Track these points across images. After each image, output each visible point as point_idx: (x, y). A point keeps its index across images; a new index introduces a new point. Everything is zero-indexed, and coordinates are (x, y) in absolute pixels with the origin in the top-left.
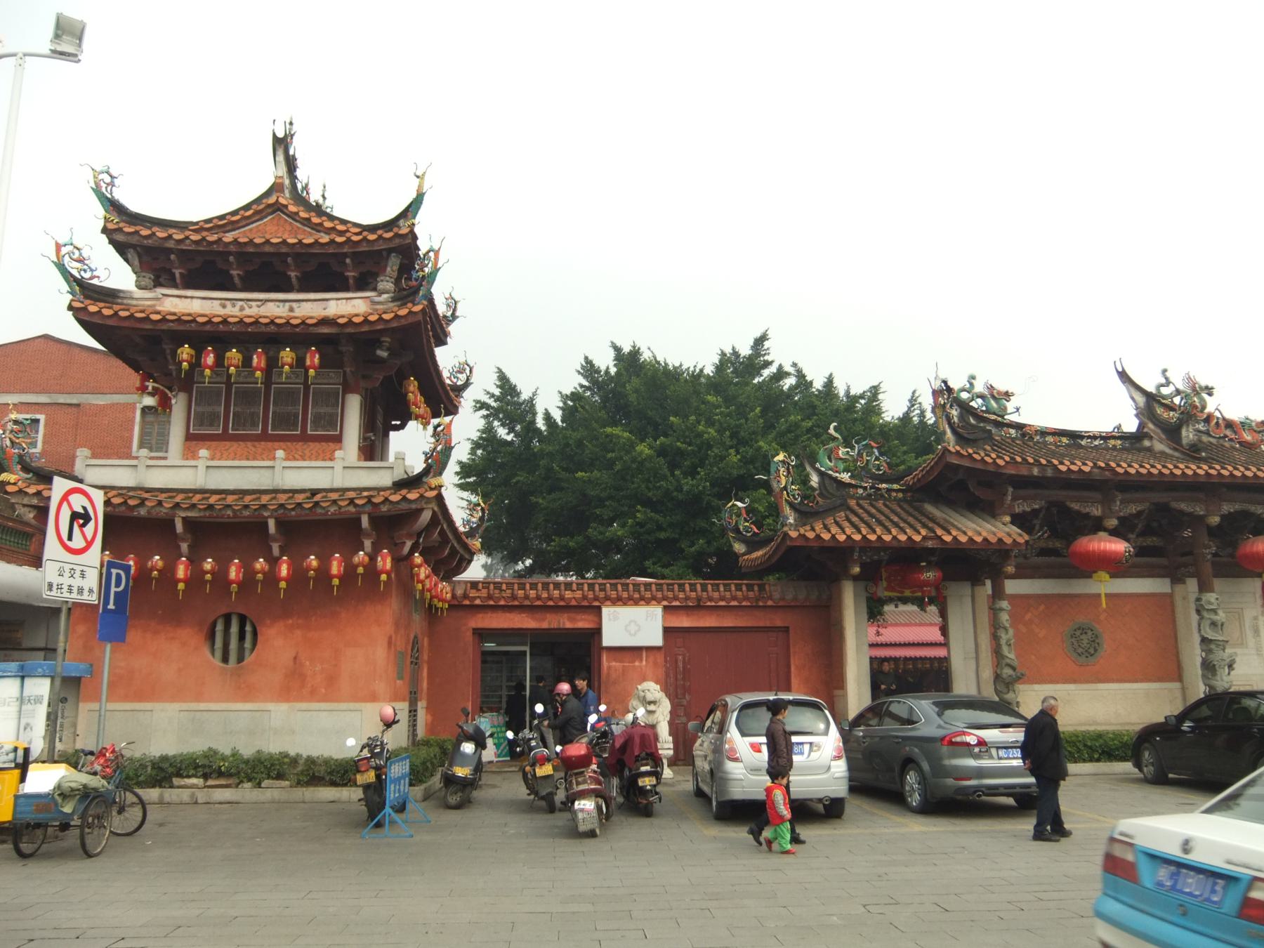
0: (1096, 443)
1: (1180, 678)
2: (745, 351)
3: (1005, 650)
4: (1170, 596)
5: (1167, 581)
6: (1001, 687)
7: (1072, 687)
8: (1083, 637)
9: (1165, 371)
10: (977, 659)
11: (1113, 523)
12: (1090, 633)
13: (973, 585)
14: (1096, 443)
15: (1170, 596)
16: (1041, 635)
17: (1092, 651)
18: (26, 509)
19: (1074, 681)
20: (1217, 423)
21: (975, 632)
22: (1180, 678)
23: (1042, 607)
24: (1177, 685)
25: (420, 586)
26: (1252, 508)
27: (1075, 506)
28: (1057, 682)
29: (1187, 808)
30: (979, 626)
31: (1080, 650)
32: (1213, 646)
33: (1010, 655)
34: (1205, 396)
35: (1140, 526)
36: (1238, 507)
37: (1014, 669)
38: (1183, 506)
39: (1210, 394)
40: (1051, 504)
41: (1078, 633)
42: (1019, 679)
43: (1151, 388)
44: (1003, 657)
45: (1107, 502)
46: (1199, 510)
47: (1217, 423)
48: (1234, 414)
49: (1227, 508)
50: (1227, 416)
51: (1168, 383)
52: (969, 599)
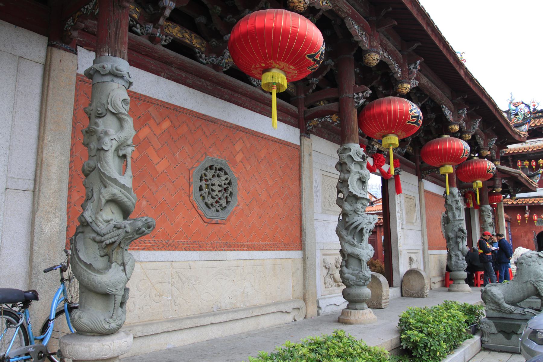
1: (300, 245)
3: (111, 166)
4: (298, 149)
6: (89, 253)
7: (194, 255)
8: (216, 181)
10: (35, 192)
12: (223, 178)
13: (50, 45)
15: (298, 149)
16: (161, 168)
17: (223, 202)
18: (127, 273)
19: (199, 247)
21: (40, 139)
22: (300, 245)
23: (166, 125)
24: (297, 254)
28: (176, 249)
29: (190, 342)
30: (50, 126)
31: (209, 201)
32: (359, 206)
33: (122, 179)
37: (126, 213)
41: (210, 174)
42: (139, 237)
44: (105, 180)
52: (38, 71)
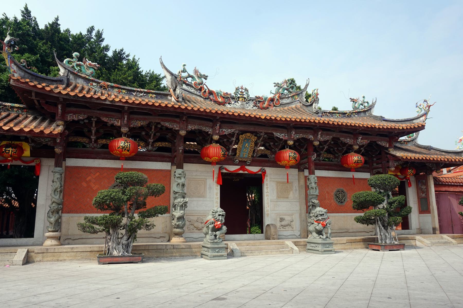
0: (142, 95)
2: (84, 33)
5: (170, 164)
9: (185, 65)
11: (291, 143)
14: (142, 95)
15: (170, 171)
20: (205, 91)
23: (98, 174)
25: (84, 184)
26: (204, 129)
27: (105, 119)
34: (203, 79)
35: (326, 148)
36: (196, 127)
38: (167, 124)
39: (206, 79)
40: (333, 139)
43: (176, 72)
45: (315, 134)
46: (176, 127)
47: (205, 91)
48: (213, 88)
49: (190, 127)
50: (211, 89)
51: (184, 71)
